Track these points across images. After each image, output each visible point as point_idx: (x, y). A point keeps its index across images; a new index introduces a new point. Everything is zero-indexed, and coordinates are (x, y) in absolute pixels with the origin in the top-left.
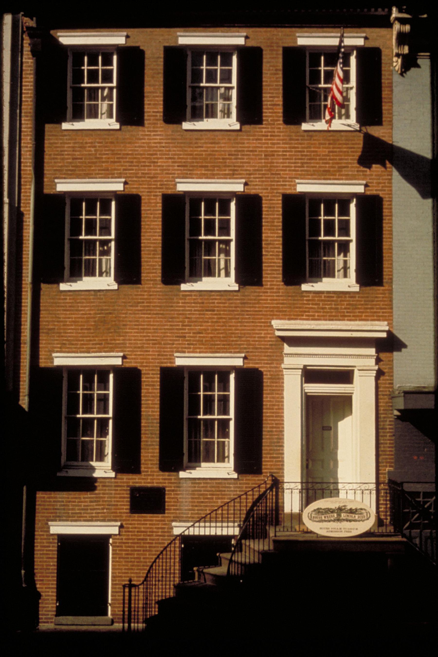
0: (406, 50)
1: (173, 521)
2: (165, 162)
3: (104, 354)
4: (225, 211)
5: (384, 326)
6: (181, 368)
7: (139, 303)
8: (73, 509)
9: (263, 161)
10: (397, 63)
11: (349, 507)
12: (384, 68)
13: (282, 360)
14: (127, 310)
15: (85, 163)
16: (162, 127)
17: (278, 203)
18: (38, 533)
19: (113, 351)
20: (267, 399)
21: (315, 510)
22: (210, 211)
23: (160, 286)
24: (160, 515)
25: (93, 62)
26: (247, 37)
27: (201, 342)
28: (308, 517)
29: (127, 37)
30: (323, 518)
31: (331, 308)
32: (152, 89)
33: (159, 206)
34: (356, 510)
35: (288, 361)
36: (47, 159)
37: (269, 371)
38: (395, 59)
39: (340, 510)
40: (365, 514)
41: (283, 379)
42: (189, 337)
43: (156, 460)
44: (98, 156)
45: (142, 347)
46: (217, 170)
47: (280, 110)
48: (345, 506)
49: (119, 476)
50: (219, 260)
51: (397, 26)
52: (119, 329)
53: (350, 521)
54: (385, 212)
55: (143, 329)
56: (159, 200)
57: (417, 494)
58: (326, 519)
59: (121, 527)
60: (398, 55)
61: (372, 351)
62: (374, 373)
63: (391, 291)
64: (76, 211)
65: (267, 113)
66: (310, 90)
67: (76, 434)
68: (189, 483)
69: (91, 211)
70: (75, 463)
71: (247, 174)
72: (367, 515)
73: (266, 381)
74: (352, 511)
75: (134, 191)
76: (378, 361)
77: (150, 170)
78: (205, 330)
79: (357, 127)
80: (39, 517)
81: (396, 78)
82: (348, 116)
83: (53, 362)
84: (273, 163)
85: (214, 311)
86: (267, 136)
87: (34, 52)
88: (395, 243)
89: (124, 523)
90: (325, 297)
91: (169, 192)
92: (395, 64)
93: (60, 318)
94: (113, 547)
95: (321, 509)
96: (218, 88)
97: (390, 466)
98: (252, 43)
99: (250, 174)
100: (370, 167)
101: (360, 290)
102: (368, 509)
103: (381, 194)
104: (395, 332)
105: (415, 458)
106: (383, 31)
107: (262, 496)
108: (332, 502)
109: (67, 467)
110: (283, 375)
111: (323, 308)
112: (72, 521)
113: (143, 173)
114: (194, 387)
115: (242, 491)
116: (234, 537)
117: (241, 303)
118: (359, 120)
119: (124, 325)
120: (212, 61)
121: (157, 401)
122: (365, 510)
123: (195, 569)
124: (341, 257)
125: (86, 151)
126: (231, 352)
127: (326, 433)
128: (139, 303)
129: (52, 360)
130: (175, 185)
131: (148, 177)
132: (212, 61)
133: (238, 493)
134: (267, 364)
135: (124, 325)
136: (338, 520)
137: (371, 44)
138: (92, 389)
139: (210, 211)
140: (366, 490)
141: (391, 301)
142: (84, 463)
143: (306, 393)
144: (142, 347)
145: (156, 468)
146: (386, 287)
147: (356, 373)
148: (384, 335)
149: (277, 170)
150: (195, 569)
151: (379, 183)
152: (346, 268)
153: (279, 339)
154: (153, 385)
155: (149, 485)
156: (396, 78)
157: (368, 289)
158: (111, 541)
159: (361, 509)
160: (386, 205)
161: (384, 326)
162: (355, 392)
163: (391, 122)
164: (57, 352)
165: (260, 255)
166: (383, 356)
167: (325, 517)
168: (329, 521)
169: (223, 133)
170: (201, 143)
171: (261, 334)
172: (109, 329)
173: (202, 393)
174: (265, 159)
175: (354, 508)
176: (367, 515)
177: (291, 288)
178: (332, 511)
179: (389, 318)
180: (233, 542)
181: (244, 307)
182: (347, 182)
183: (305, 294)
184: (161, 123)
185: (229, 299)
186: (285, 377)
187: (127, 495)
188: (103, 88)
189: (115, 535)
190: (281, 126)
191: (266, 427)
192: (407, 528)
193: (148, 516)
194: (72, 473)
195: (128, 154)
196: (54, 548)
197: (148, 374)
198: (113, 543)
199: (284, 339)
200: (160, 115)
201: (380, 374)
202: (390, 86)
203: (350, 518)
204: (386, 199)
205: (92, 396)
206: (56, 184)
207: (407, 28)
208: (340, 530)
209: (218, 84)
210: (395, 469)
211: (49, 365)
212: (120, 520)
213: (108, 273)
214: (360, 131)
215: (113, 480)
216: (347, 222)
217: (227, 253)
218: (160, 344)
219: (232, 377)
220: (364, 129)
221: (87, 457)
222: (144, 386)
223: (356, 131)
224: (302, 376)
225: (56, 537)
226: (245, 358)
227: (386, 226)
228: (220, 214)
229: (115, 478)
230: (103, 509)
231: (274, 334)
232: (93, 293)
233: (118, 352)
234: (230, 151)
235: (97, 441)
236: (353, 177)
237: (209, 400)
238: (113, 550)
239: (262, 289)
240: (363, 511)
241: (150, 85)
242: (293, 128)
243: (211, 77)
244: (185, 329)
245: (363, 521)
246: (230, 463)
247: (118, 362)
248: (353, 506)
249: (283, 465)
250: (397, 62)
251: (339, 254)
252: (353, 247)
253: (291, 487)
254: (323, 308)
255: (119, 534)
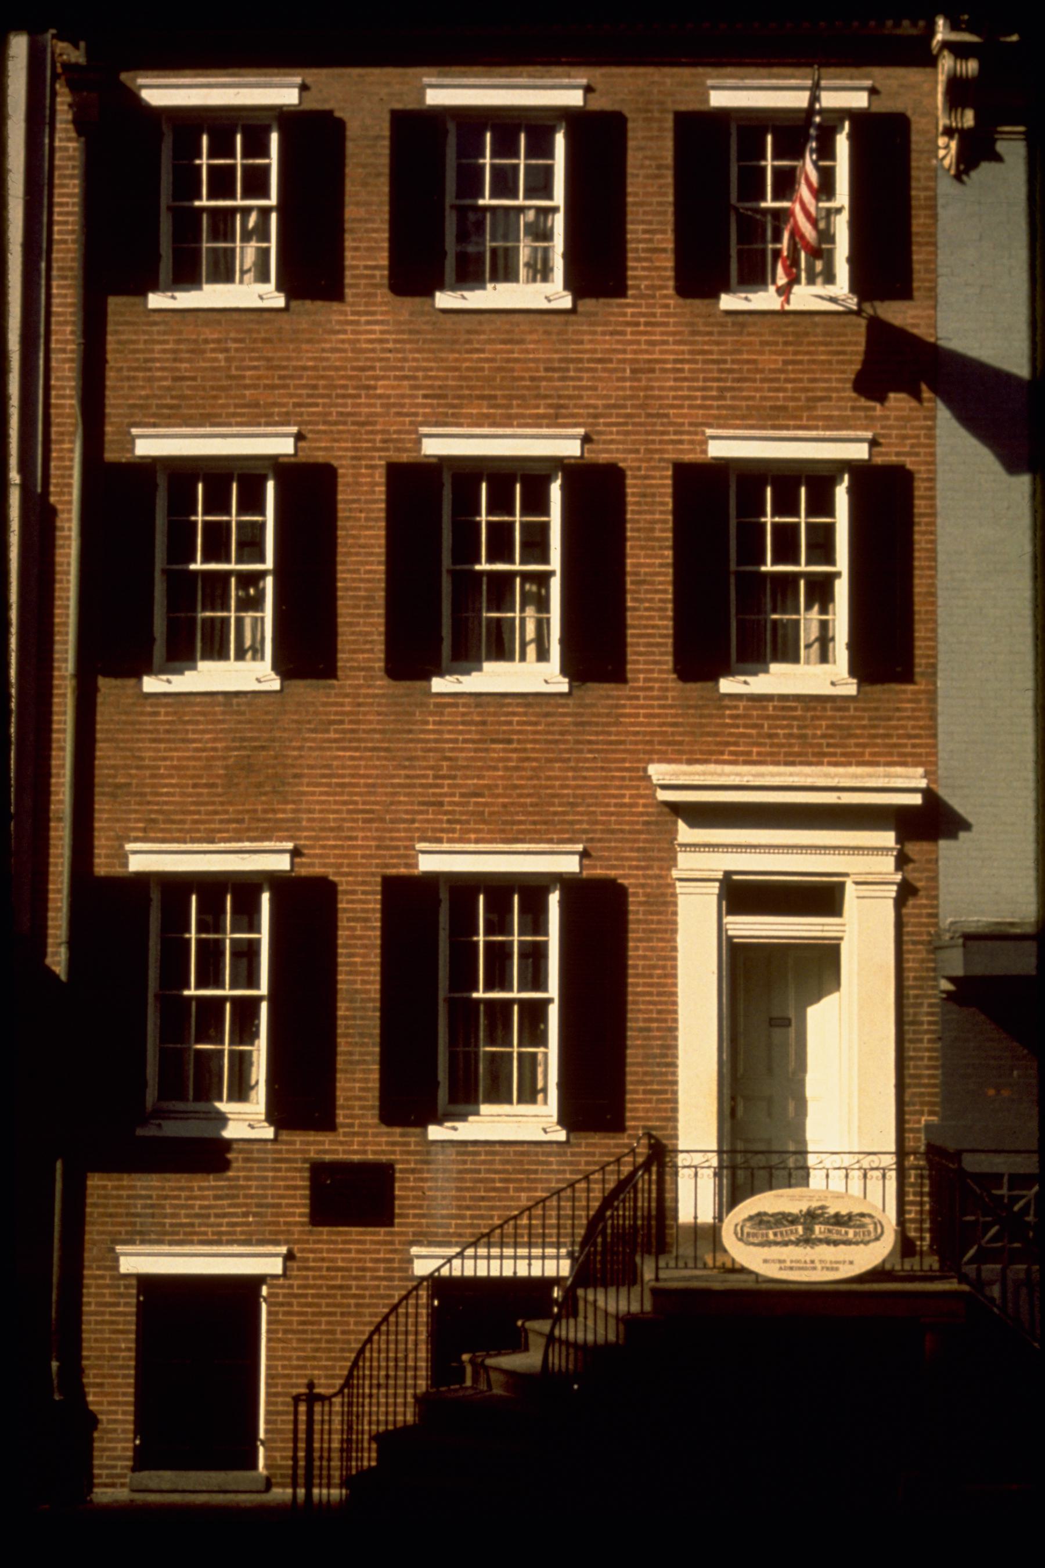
0: (969, 119)
1: (413, 1243)
2: (393, 387)
3: (247, 845)
4: (537, 503)
5: (915, 777)
6: (433, 879)
7: (332, 722)
8: (174, 1215)
9: (628, 384)
10: (947, 151)
11: (832, 1211)
12: (917, 162)
13: (673, 862)
14: (305, 740)
15: (204, 389)
16: (386, 304)
17: (664, 482)
18: (90, 1272)
19: (269, 839)
20: (637, 951)
21: (751, 1218)
22: (501, 503)
23: (382, 684)
24: (383, 1230)
25: (222, 147)
26: (588, 90)
27: (479, 816)
28: (736, 1233)
29: (304, 88)
30: (771, 1237)
31: (790, 736)
32: (362, 212)
33: (381, 489)
34: (850, 1216)
35: (686, 863)
36: (111, 378)
37: (643, 886)
38: (942, 141)
39: (812, 1217)
40: (871, 1227)
41: (675, 904)
42: (451, 803)
43: (373, 1099)
44: (234, 372)
45: (340, 829)
46: (519, 406)
47: (667, 262)
48: (823, 1207)
49: (285, 1136)
50: (523, 621)
51: (947, 63)
52: (284, 784)
53: (836, 1243)
54: (920, 505)
55: (343, 785)
56: (380, 477)
57: (996, 1179)
58: (779, 1239)
59: (289, 1257)
60: (949, 132)
61: (888, 838)
62: (892, 891)
63: (932, 696)
64: (183, 505)
65: (636, 270)
66: (740, 217)
67: (184, 1038)
68: (452, 1153)
69: (217, 503)
70: (180, 1106)
71: (589, 415)
72: (875, 1229)
73: (635, 910)
74: (839, 1220)
75: (320, 457)
76: (902, 860)
77: (359, 405)
78: (489, 787)
79: (853, 303)
80: (93, 1233)
81: (946, 186)
82: (830, 278)
83: (126, 865)
84: (652, 388)
85: (509, 741)
86: (637, 324)
87: (80, 124)
88: (943, 579)
89: (296, 1248)
90: (775, 708)
91: (404, 457)
92: (942, 153)
93: (142, 759)
94: (269, 1305)
95: (765, 1214)
96: (521, 209)
97: (931, 1113)
98: (600, 103)
99: (596, 416)
100: (882, 399)
101: (859, 691)
102: (878, 1215)
103: (909, 463)
104: (943, 793)
105: (991, 1092)
106: (913, 75)
107: (626, 1184)
108: (792, 1198)
109: (161, 1114)
110: (674, 895)
111: (770, 736)
112: (171, 1243)
113: (341, 414)
114: (465, 924)
115: (578, 1172)
116: (557, 1281)
117: (576, 724)
118: (857, 285)
119: (295, 776)
120: (505, 147)
121: (375, 957)
122: (870, 1216)
123: (465, 1357)
124: (815, 614)
125: (204, 360)
126: (550, 841)
127: (777, 1032)
128: (332, 722)
129: (123, 858)
130: (418, 442)
131: (354, 423)
132: (505, 147)
133: (568, 1176)
134: (637, 868)
135: (295, 776)
136: (807, 1241)
137: (885, 105)
138: (219, 928)
139: (501, 503)
140: (872, 1169)
141: (933, 717)
142: (201, 1106)
143: (730, 938)
144: (340, 829)
145: (372, 1117)
146: (921, 685)
147: (851, 891)
148: (917, 799)
149: (661, 407)
150: (465, 1357)
151: (905, 437)
152: (825, 640)
153: (666, 810)
154: (366, 920)
155: (356, 1158)
156: (946, 186)
157: (877, 690)
158: (264, 1291)
159: (862, 1215)
160: (920, 488)
161: (915, 777)
162: (846, 936)
163: (932, 292)
164: (136, 840)
165: (620, 609)
166: (913, 849)
167: (775, 1234)
168: (786, 1244)
169: (532, 317)
170: (478, 342)
171: (623, 796)
172: (259, 785)
173: (481, 938)
174: (631, 379)
175: (844, 1212)
176: (875, 1229)
177: (695, 688)
178: (791, 1220)
179: (927, 760)
180: (556, 1293)
181: (583, 733)
182: (828, 434)
183: (727, 702)
184: (383, 294)
185: (547, 715)
186: (681, 900)
187: (302, 1181)
188: (246, 211)
189: (275, 1277)
190: (671, 302)
191: (636, 1018)
192: (971, 1261)
193: (355, 1232)
194: (172, 1129)
195: (305, 368)
196: (128, 1307)
197: (353, 892)
198: (270, 1295)
199: (677, 809)
200: (382, 275)
201: (906, 892)
202: (932, 206)
203: (835, 1237)
204: (921, 473)
205: (219, 944)
206: (133, 439)
207: (972, 66)
208: (812, 1266)
209: (520, 202)
210: (943, 1119)
211: (117, 871)
212: (286, 1242)
213: (257, 653)
214: (858, 313)
215: (269, 1146)
216: (829, 530)
217: (543, 605)
218: (382, 820)
219: (554, 899)
220: (868, 308)
221: (208, 1091)
222: (343, 922)
223: (849, 312)
224: (720, 897)
225: (134, 1282)
226: (584, 855)
227: (920, 540)
228: (526, 510)
229: (275, 1140)
230: (246, 1215)
231: (654, 796)
232: (221, 699)
233: (281, 839)
234: (549, 360)
235: (232, 1053)
236: (843, 423)
237: (498, 955)
238: (269, 1313)
239: (625, 690)
240: (867, 1220)
241: (357, 204)
242: (698, 305)
243: (504, 184)
244: (441, 786)
245: (866, 1243)
246: (550, 1107)
247: (281, 863)
248: (843, 1208)
249: (675, 1110)
250: (947, 147)
251: (809, 607)
252: (842, 589)
253: (882, 1165)
254: (770, 736)
255: (284, 1275)
